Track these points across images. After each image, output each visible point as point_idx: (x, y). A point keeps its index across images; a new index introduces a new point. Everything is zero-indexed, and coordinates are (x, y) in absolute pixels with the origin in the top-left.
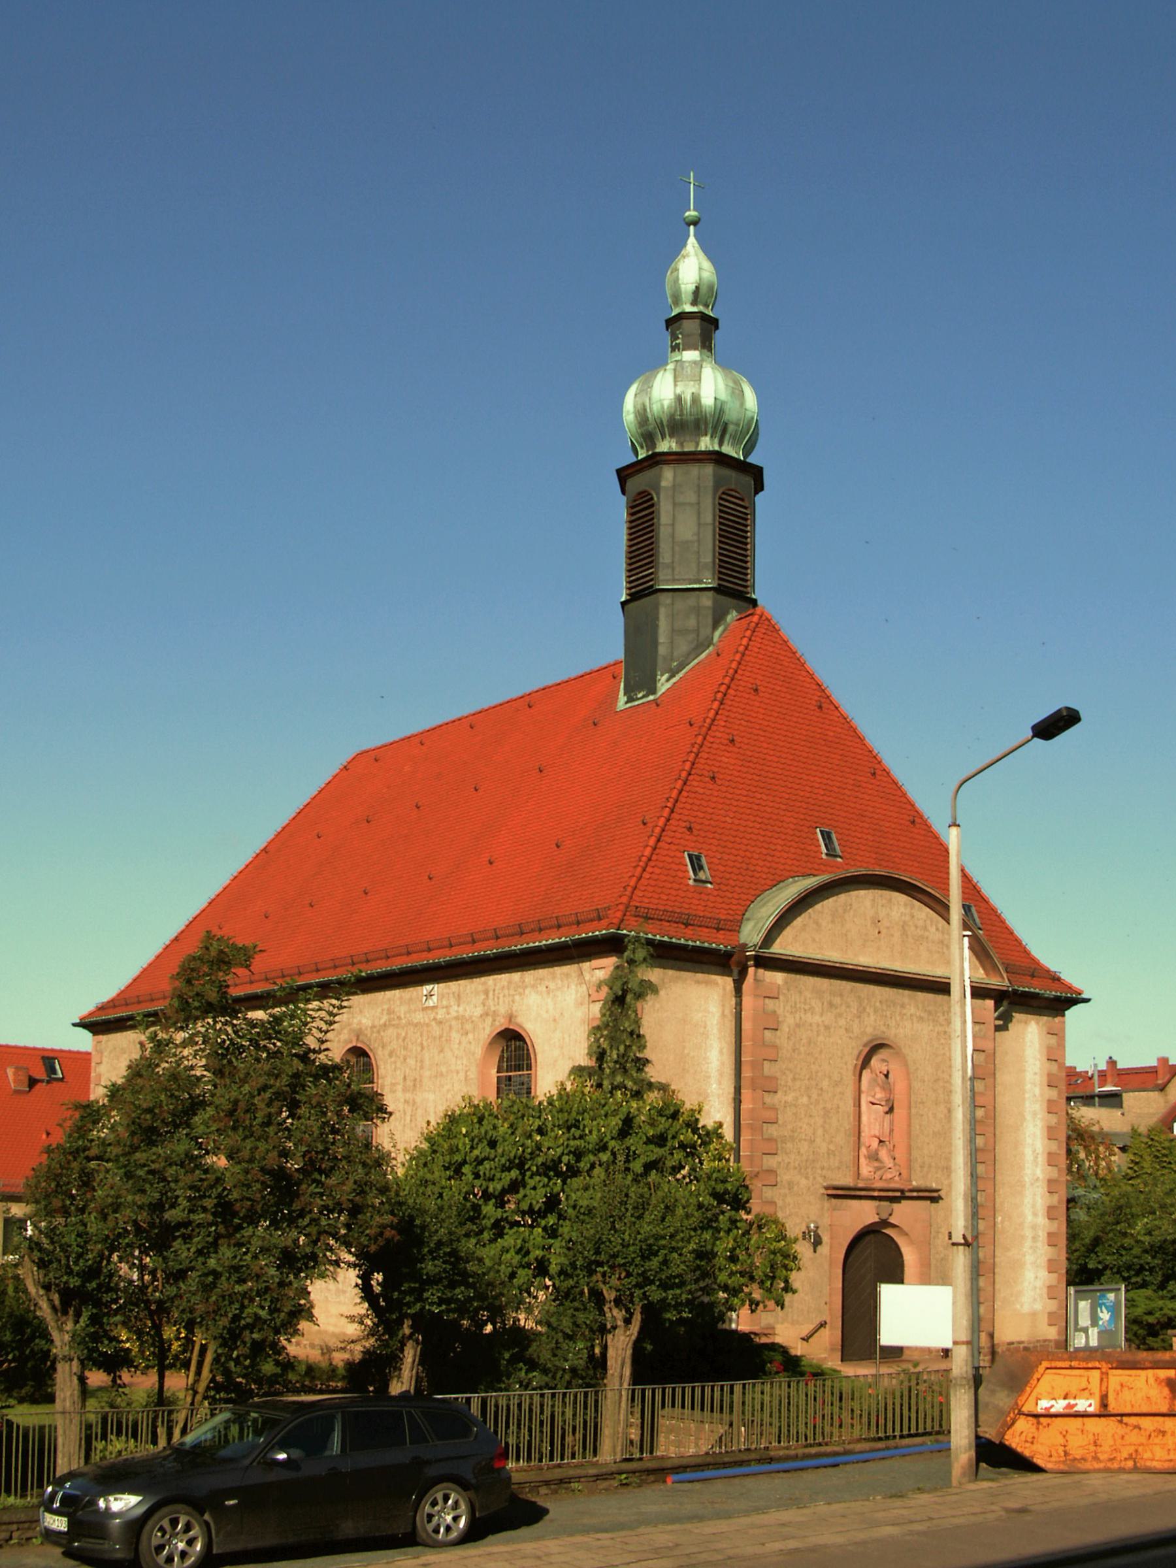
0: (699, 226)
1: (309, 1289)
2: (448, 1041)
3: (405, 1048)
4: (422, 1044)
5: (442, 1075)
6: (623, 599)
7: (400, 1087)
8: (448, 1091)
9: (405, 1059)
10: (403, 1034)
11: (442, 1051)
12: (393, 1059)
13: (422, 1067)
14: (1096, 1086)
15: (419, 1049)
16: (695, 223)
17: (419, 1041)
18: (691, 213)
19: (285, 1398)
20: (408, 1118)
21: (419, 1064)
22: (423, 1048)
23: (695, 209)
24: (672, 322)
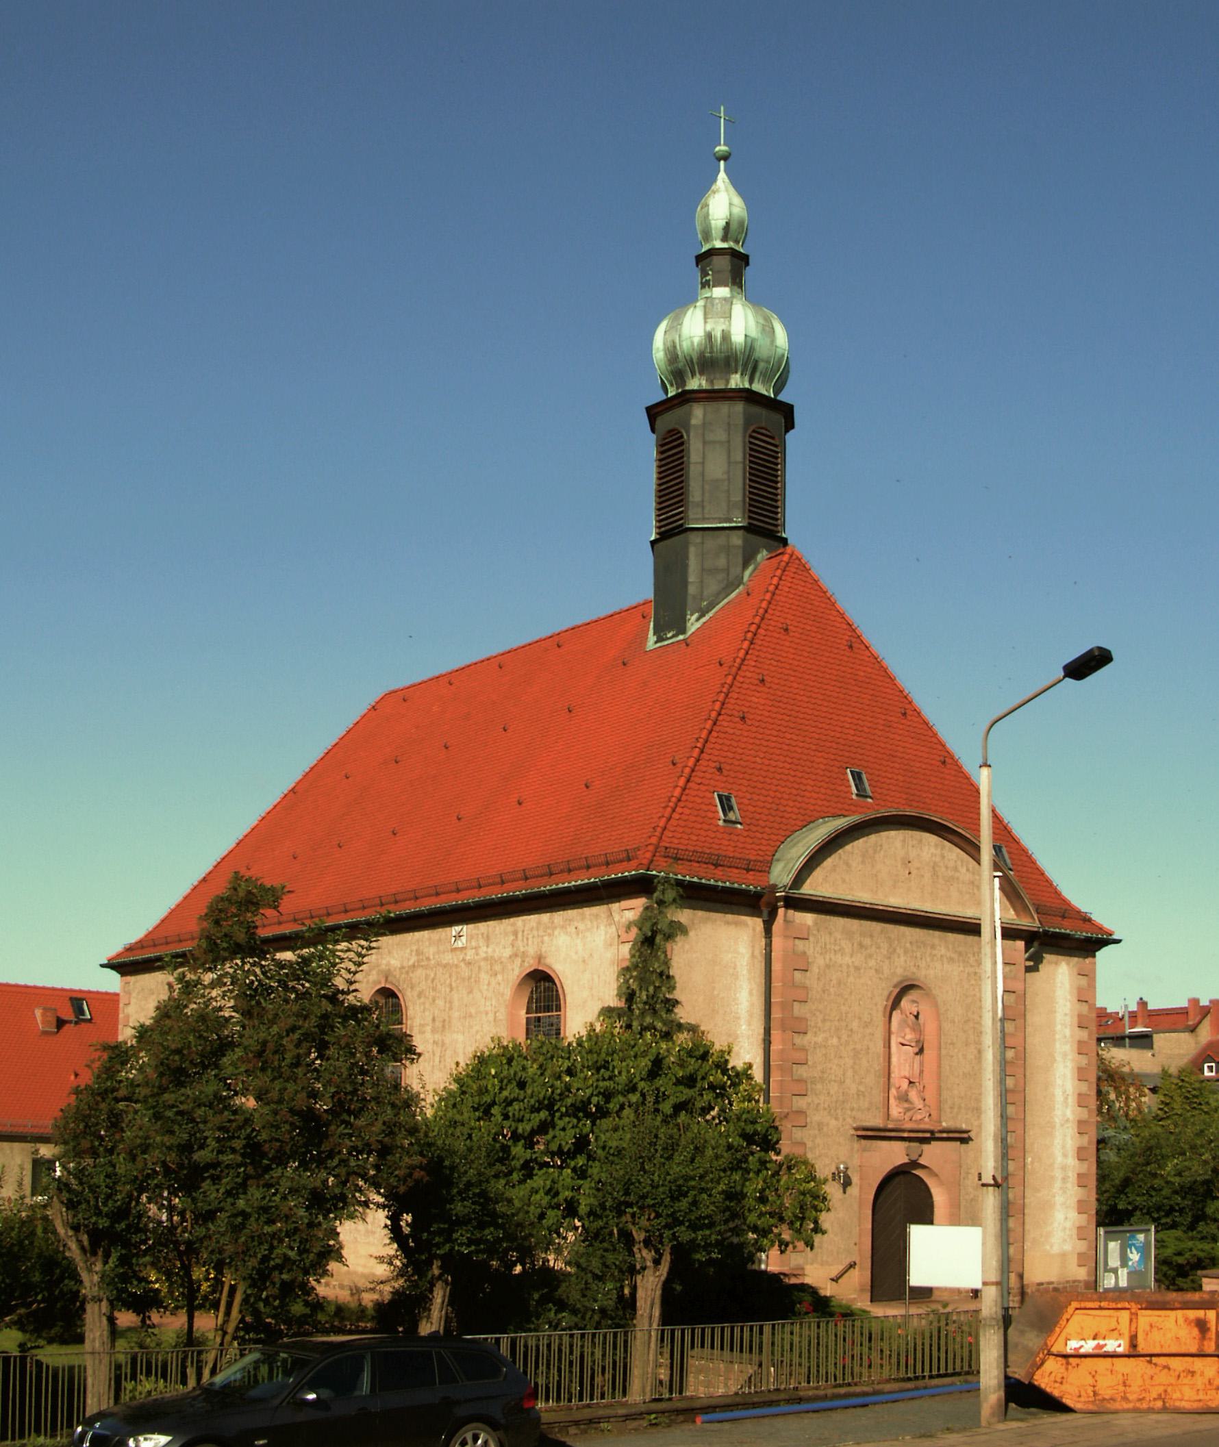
3: (434, 989)
5: (471, 1016)
7: (428, 1028)
10: (432, 975)
13: (451, 1008)
14: (1127, 1027)
15: (448, 990)
16: (725, 158)
17: (448, 982)
18: (722, 148)
20: (437, 1060)
21: (448, 1005)
22: (452, 989)
23: (725, 144)
24: (702, 259)
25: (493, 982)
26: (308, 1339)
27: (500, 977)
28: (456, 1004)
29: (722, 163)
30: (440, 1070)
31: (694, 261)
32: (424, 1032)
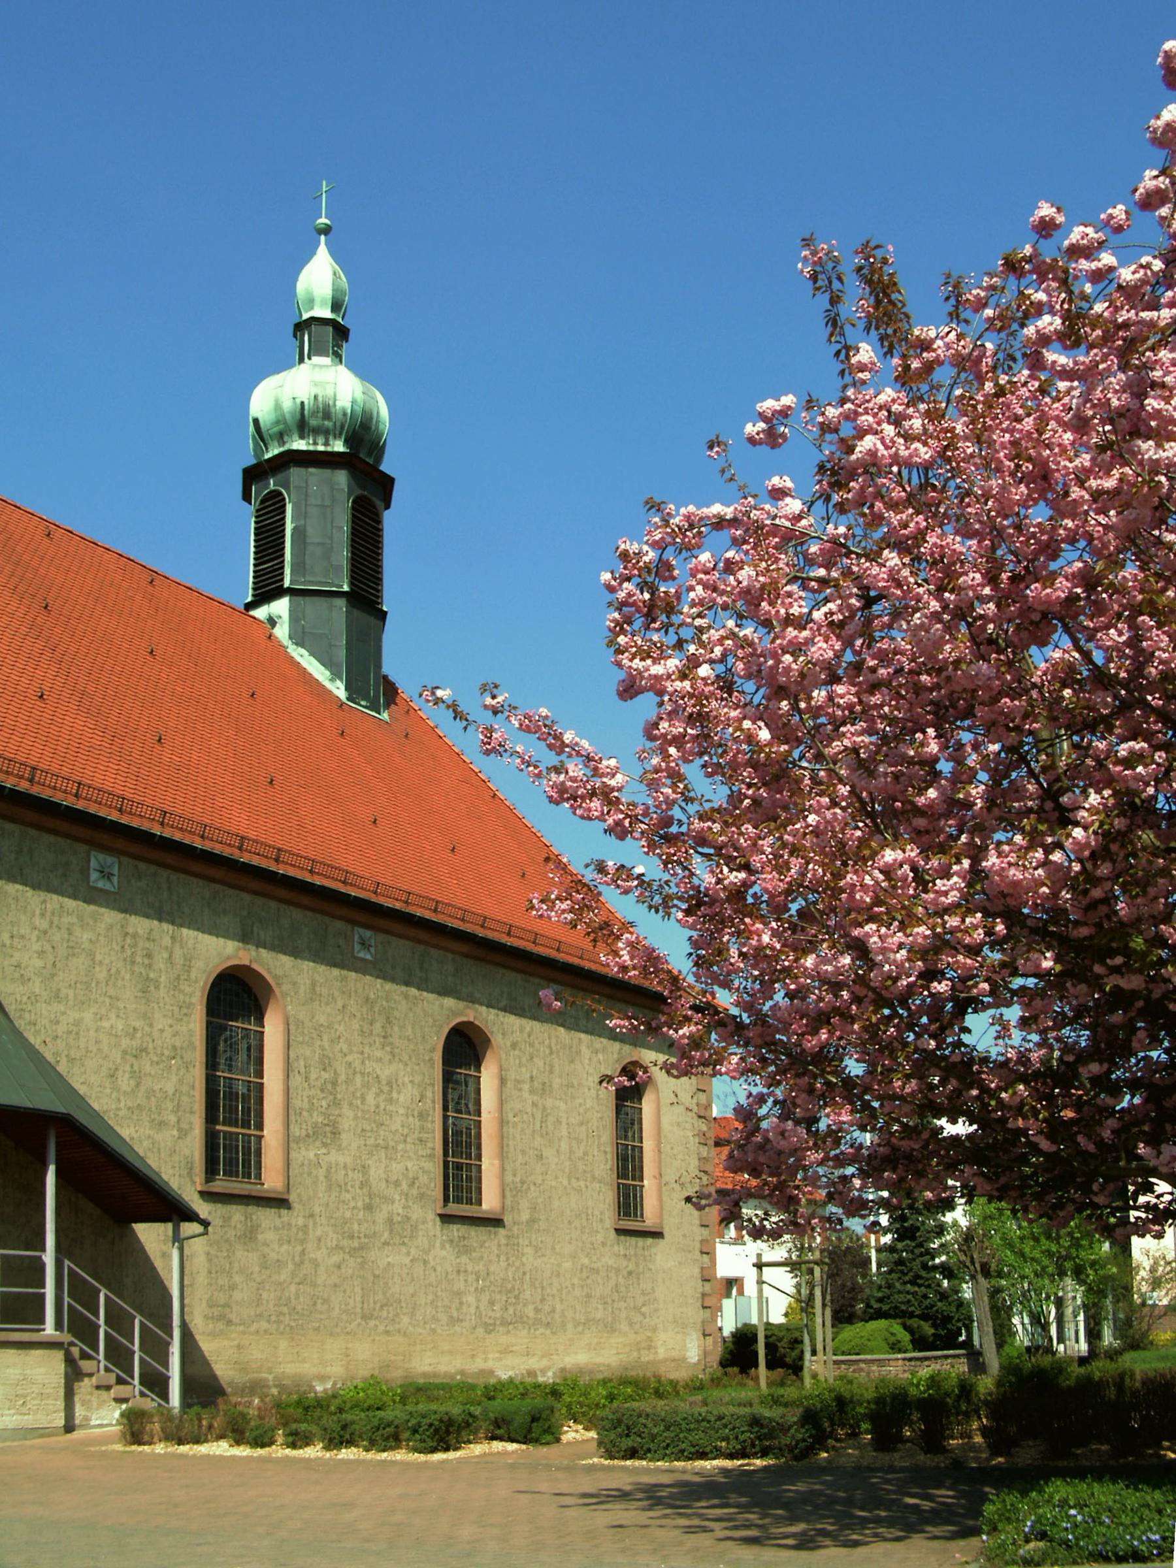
0: (330, 236)
1: (1148, 1236)
2: (579, 1053)
3: (532, 1045)
4: (550, 1047)
5: (573, 1087)
6: (249, 599)
7: (526, 1087)
8: (580, 1105)
9: (531, 1058)
10: (528, 1029)
11: (572, 1061)
12: (517, 1052)
13: (551, 1072)
14: (72, 1265)
15: (547, 1052)
16: (326, 231)
17: (547, 1042)
18: (323, 220)
19: (92, 1449)
20: (538, 1125)
21: (547, 1068)
22: (551, 1053)
23: (326, 217)
24: (301, 327)
25: (595, 1059)
26: (103, 1448)
27: (600, 1056)
28: (557, 1069)
29: (323, 238)
30: (542, 1136)
31: (777, 451)
32: (520, 1090)
